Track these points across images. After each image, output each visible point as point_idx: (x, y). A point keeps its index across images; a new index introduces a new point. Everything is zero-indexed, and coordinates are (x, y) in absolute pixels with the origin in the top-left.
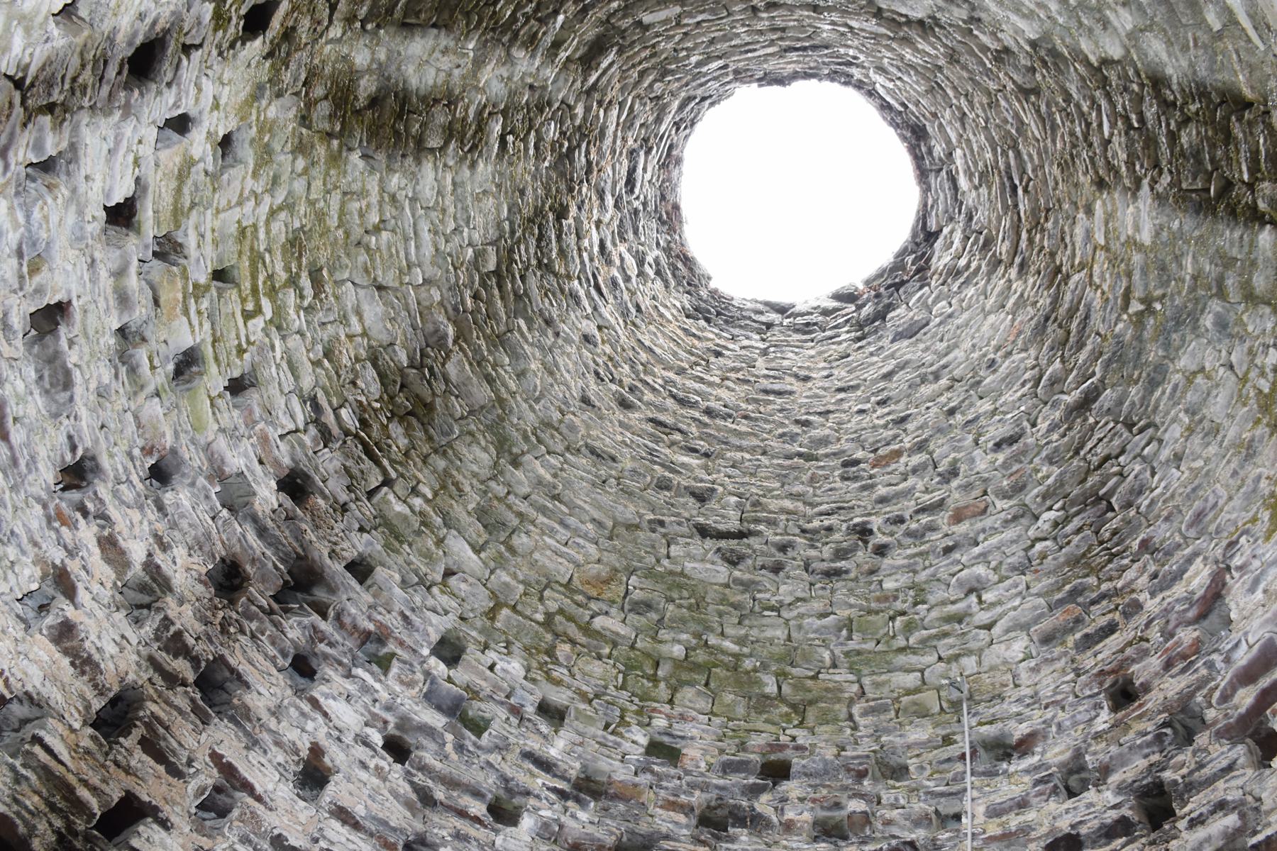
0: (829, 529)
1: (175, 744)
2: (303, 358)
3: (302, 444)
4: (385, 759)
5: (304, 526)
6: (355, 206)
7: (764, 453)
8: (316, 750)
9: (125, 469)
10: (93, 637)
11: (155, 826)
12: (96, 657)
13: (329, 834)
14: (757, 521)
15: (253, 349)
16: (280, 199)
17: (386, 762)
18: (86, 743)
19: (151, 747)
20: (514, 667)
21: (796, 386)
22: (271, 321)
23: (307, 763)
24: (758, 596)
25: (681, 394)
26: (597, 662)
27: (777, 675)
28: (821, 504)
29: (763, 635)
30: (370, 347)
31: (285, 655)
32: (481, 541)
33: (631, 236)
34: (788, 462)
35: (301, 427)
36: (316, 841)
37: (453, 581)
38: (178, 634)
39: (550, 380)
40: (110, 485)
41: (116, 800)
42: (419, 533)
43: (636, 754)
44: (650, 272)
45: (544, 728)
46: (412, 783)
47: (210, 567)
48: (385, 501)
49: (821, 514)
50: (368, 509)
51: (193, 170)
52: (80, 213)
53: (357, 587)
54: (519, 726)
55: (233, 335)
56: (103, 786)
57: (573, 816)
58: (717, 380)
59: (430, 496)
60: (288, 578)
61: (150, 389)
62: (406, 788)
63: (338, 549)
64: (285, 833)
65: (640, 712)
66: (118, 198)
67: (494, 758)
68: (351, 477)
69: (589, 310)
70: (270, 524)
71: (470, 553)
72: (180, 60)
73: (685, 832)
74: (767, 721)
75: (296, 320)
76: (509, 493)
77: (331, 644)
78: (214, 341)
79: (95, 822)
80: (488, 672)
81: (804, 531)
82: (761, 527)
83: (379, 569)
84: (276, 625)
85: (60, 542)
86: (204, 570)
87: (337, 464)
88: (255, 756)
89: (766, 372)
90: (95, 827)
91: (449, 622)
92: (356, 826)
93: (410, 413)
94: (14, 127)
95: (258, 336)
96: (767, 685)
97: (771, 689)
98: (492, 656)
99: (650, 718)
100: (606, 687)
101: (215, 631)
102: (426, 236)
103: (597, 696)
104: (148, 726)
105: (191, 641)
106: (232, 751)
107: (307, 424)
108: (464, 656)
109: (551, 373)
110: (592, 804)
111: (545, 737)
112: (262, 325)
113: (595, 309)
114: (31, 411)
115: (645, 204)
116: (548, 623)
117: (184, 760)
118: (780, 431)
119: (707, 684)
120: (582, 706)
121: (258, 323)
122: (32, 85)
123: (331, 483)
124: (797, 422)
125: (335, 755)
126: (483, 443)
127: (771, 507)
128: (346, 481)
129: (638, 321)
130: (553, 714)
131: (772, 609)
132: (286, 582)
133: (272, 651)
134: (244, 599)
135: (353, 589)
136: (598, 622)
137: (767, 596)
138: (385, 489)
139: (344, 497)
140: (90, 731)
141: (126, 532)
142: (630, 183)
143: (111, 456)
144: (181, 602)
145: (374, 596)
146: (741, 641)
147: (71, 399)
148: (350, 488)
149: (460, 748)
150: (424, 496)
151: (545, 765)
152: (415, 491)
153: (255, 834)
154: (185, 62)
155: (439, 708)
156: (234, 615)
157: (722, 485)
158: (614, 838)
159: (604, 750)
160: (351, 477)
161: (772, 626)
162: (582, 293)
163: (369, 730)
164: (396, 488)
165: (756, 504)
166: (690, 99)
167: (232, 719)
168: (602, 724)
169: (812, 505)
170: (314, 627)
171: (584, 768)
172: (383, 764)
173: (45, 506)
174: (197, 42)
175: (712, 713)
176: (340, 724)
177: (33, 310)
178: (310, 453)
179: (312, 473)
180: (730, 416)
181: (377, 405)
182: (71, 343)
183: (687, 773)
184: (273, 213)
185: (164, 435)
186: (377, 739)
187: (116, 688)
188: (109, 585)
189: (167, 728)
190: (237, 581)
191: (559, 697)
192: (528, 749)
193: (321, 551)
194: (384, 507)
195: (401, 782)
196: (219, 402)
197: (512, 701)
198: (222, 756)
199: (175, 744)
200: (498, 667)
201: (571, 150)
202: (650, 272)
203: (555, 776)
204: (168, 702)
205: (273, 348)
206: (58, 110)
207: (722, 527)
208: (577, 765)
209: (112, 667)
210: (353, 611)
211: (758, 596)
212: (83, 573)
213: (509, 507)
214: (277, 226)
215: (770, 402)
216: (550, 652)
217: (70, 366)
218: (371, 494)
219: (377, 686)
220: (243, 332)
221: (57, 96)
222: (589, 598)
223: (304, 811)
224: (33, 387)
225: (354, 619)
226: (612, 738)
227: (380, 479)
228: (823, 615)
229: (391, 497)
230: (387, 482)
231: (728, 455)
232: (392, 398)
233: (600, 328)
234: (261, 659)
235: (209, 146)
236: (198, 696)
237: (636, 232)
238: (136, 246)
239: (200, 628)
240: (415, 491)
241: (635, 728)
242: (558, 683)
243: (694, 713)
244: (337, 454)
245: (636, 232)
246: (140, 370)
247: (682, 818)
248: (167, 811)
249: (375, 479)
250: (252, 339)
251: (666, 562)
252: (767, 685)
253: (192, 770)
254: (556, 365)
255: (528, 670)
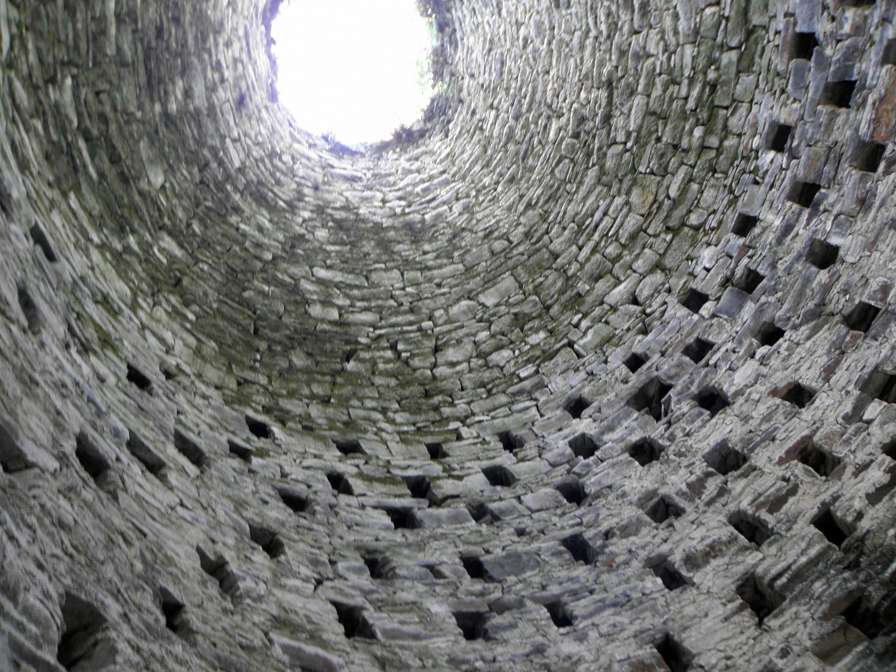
0: (609, 15)
1: (773, 489)
2: (488, 404)
3: (546, 402)
4: (780, 346)
5: (605, 401)
6: (381, 366)
7: (548, 72)
8: (774, 393)
9: (572, 518)
10: (695, 543)
11: (837, 504)
12: (708, 541)
13: (843, 382)
14: (600, 74)
15: (482, 435)
16: (379, 416)
17: (782, 343)
18: (773, 550)
19: (776, 503)
20: (707, 255)
21: (497, 51)
22: (462, 422)
23: (784, 398)
24: (658, 71)
25: (504, 139)
26: (705, 194)
27: (722, 52)
28: (588, 24)
29: (690, 66)
30: (477, 356)
31: (701, 414)
32: (612, 280)
33: (392, 179)
34: (555, 53)
35: (534, 403)
36: (848, 393)
37: (641, 299)
38: (689, 485)
39: (496, 234)
40: (584, 529)
41: (817, 530)
42: (607, 323)
43: (782, 159)
44: (416, 165)
45: (757, 230)
46: (801, 325)
47: (637, 463)
48: (584, 347)
49: (596, 23)
50: (589, 357)
51: (365, 472)
52: (400, 545)
53: (648, 364)
54: (754, 248)
55: (473, 447)
56: (807, 539)
57: (832, 205)
58: (493, 113)
59: (580, 316)
60: (643, 412)
61: (515, 502)
62: (805, 330)
63: (620, 378)
64: (842, 414)
65: (746, 158)
66: (387, 520)
67: (781, 267)
68: (567, 369)
69: (445, 207)
70: (605, 423)
71: (621, 287)
72: (293, 479)
73: (852, 116)
74: (761, 56)
75: (461, 407)
76: (577, 260)
77: (692, 383)
78: (479, 459)
79: (834, 546)
80: (712, 272)
81: (609, 37)
82: (605, 71)
83: (634, 350)
84: (678, 419)
85: (627, 563)
86: (640, 468)
87: (559, 380)
88: (780, 435)
89: (487, 75)
90: (839, 544)
91: (672, 300)
92: (837, 363)
93: (522, 330)
94: (348, 586)
95: (474, 431)
96: (730, 59)
97: (733, 55)
98: (698, 269)
99: (752, 150)
100: (725, 186)
101: (685, 462)
102: (400, 319)
103: (731, 191)
104: (758, 508)
105: (693, 478)
106: (778, 452)
107: (531, 399)
108: (699, 290)
109: (491, 232)
110: (823, 191)
111: (764, 230)
112: (466, 428)
113: (444, 203)
114: (537, 579)
115: (369, 169)
116: (674, 231)
117: (785, 484)
118: (531, 61)
119: (727, 108)
120: (740, 203)
121: (464, 431)
122: (319, 573)
123: (573, 384)
124: (525, 47)
125: (781, 378)
126: (541, 279)
127: (589, 64)
128: (571, 373)
129: (452, 172)
130: (746, 224)
131: (669, 59)
132: (647, 413)
133: (698, 423)
134: (660, 441)
135: (650, 368)
136: (673, 193)
137: (658, 64)
138: (576, 346)
139: (582, 374)
140: (764, 547)
141: (616, 520)
142: (353, 179)
143: (563, 528)
144: (664, 483)
145: (654, 352)
146: (692, 81)
147: (526, 553)
148: (577, 370)
149: (774, 291)
150: (580, 320)
151: (787, 229)
152: (577, 326)
153: (843, 435)
154: (293, 476)
155: (741, 307)
156: (672, 448)
157: (572, 104)
158: (854, 172)
159: (777, 184)
160: (567, 369)
161: (682, 59)
162: (434, 212)
163: (758, 356)
164: (575, 339)
165: (586, 77)
166: (292, 136)
167: (752, 450)
168: (756, 187)
169: (588, 31)
170: (679, 393)
171: (790, 198)
172: (785, 345)
173: (603, 572)
174: (278, 469)
175: (751, 102)
176: (754, 376)
177: (468, 577)
178: (552, 397)
179: (567, 396)
180: (520, 101)
181: (517, 352)
182: (488, 552)
183: (802, 118)
184: (392, 422)
185: (546, 494)
186: (764, 350)
187: (731, 529)
188: (655, 532)
189: (760, 495)
190: (646, 446)
191: (731, 219)
192: (774, 242)
193: (626, 390)
194: (589, 347)
195: (800, 332)
196: (520, 455)
197: (735, 255)
198: (781, 458)
199: (773, 489)
200: (707, 266)
201: (334, 220)
202: (416, 165)
203: (797, 220)
204: (740, 494)
205: (480, 422)
206: (333, 558)
207: (604, 104)
208: (789, 204)
209: (716, 531)
210: (666, 367)
211: (658, 71)
212: (648, 548)
213: (588, 259)
214: (399, 418)
215: (510, 71)
216: (697, 228)
217: (504, 553)
218: (579, 356)
219: (723, 350)
220: (471, 441)
221: (324, 558)
222: (655, 201)
223: (822, 400)
224: (520, 578)
225: (672, 367)
226: (767, 179)
227: (569, 349)
228: (676, 17)
229: (581, 342)
230: (571, 344)
231: (549, 101)
232: (512, 342)
233: (458, 199)
234: (704, 430)
235: (349, 462)
236: (735, 473)
237: (390, 175)
238: (421, 509)
239: (682, 471)
240: (577, 326)
241: (760, 162)
242: (720, 223)
243: (750, 116)
244: (552, 378)
245: (390, 175)
246: (503, 508)
247: (840, 120)
248: (826, 497)
249: (566, 353)
250: (475, 434)
251: (629, 145)
252: (730, 59)
253: (792, 478)
254: (486, 229)
255: (709, 244)
